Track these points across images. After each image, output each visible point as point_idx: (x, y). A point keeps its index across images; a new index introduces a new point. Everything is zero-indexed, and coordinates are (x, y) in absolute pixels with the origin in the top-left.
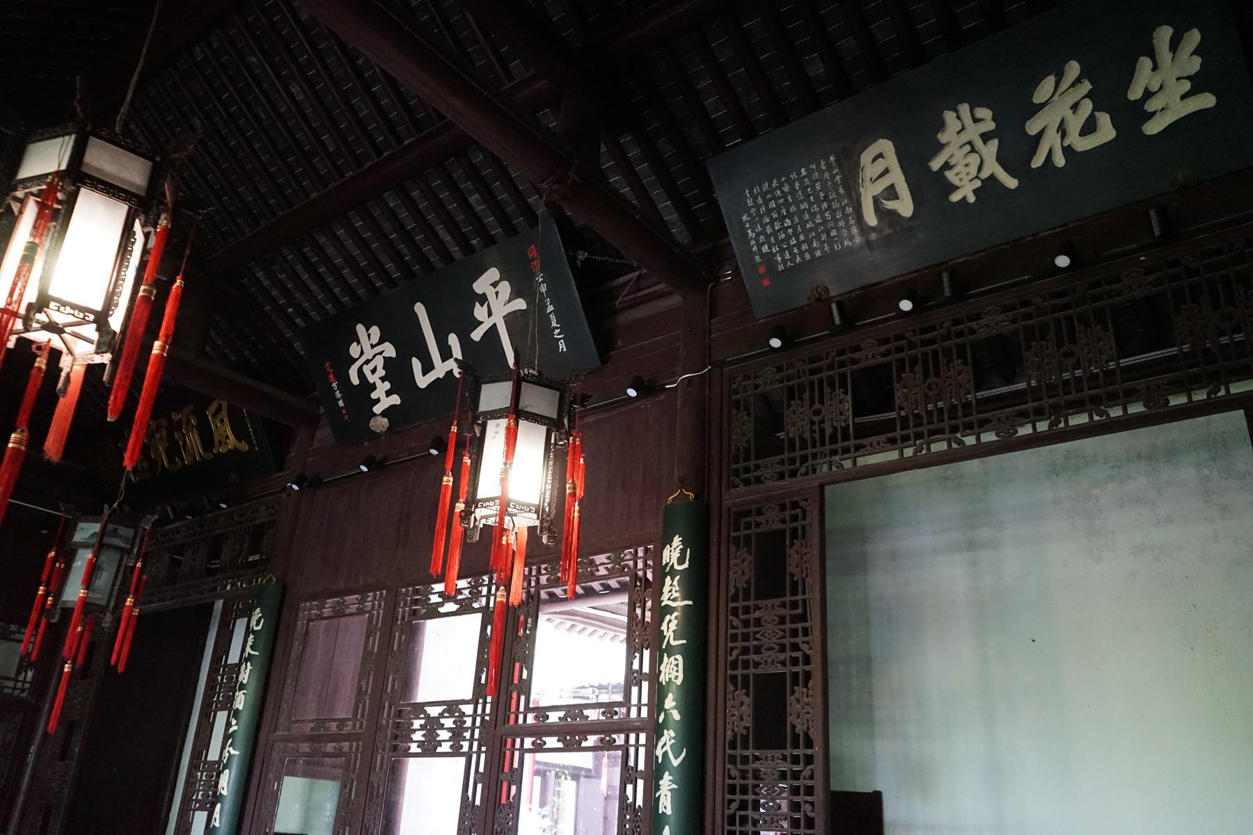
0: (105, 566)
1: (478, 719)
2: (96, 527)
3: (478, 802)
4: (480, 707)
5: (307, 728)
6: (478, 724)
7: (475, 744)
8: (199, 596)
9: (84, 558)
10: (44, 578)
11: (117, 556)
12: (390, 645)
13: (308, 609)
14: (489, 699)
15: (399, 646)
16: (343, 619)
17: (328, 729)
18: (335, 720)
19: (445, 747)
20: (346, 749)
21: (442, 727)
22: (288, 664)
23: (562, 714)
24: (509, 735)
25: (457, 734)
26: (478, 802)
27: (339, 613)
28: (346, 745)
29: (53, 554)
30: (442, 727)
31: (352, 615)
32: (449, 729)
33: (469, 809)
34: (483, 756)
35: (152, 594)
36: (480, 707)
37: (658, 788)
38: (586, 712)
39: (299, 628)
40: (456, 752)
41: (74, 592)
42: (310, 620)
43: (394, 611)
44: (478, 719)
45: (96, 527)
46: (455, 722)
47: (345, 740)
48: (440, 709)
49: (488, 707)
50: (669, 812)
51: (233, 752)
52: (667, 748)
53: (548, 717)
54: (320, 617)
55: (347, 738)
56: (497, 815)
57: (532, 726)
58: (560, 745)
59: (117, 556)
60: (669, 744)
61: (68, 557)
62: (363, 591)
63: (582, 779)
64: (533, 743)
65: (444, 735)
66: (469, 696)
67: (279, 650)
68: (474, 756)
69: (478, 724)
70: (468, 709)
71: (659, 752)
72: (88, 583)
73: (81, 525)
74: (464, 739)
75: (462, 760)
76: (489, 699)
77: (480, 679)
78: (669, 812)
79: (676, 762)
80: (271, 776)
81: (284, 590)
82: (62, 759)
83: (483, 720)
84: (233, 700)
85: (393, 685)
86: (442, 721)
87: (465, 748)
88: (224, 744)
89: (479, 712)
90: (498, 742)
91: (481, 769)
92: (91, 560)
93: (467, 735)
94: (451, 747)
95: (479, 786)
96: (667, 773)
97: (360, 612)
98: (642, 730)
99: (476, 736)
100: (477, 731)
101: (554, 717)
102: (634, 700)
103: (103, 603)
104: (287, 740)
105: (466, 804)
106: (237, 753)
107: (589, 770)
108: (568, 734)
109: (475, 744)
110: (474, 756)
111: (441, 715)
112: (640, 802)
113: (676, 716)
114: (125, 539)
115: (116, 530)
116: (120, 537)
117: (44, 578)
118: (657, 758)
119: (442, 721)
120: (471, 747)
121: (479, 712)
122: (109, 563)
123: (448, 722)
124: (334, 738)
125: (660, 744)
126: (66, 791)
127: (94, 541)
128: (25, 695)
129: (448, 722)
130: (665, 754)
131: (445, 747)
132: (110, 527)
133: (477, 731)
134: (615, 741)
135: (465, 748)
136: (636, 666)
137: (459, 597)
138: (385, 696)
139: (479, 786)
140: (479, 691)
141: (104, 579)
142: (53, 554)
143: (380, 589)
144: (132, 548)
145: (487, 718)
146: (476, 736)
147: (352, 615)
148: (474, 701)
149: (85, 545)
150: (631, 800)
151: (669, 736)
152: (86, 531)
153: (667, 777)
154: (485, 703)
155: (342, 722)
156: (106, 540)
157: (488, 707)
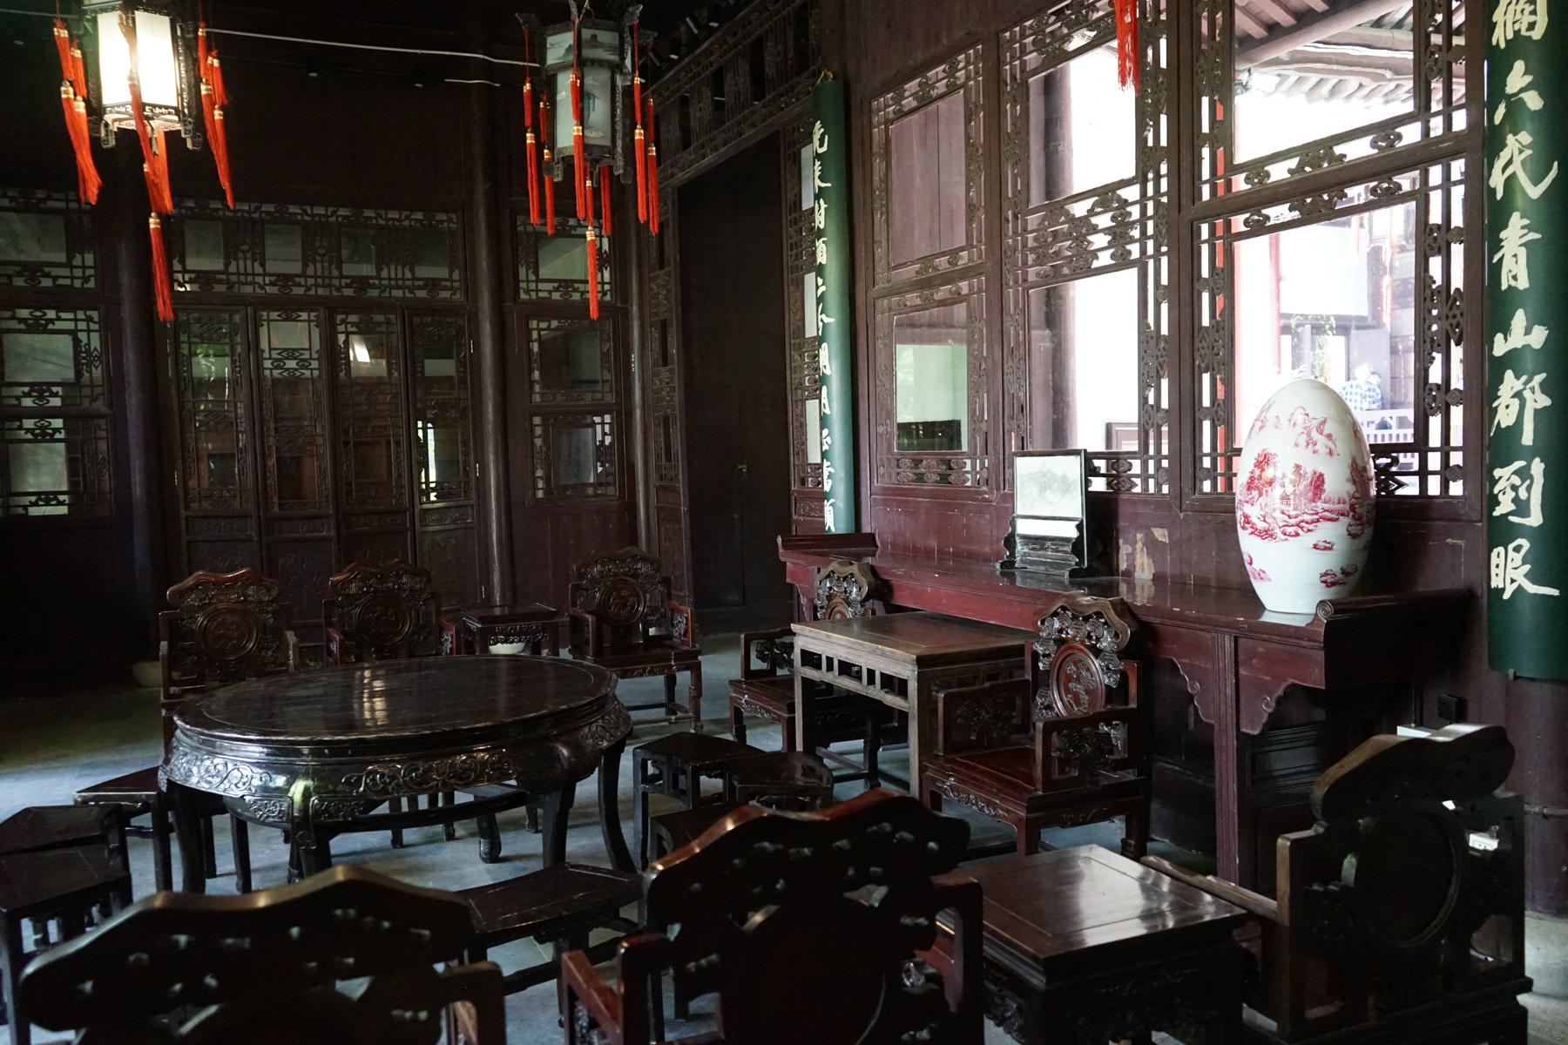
0: (597, 93)
1: (1150, 205)
2: (568, 39)
3: (1164, 331)
4: (1150, 186)
5: (909, 272)
6: (1150, 212)
7: (1150, 244)
8: (752, 131)
9: (566, 81)
10: (528, 121)
11: (605, 75)
12: (1000, 126)
13: (884, 106)
14: (1164, 169)
15: (1014, 125)
16: (932, 107)
17: (935, 269)
18: (943, 254)
19: (1105, 259)
20: (965, 291)
21: (1095, 230)
22: (873, 192)
23: (1293, 163)
24: (1203, 220)
25: (1119, 235)
26: (1164, 331)
27: (925, 101)
28: (964, 286)
29: (527, 87)
30: (1095, 230)
31: (941, 97)
32: (1106, 231)
33: (1152, 343)
34: (1164, 260)
35: (703, 147)
36: (1150, 186)
37: (1497, 245)
38: (1338, 150)
39: (876, 138)
40: (1122, 262)
41: (567, 133)
42: (888, 122)
43: (999, 71)
44: (1150, 205)
45: (568, 39)
46: (1113, 218)
47: (962, 279)
48: (1087, 204)
49: (1164, 183)
50: (1523, 283)
51: (826, 320)
52: (1516, 167)
53: (1268, 175)
54: (901, 114)
55: (966, 273)
56: (1197, 345)
57: (1246, 194)
58: (1296, 214)
59: (605, 75)
60: (1518, 160)
61: (546, 86)
62: (948, 57)
63: (1353, 332)
64: (1246, 223)
65: (1099, 240)
66: (1130, 171)
67: (857, 177)
68: (1151, 263)
69: (1150, 212)
70: (1131, 193)
71: (1497, 181)
72: (581, 118)
73: (550, 40)
74: (1132, 240)
75: (1133, 273)
76: (1164, 169)
77: (1146, 139)
78: (1523, 283)
79: (1535, 192)
80: (880, 344)
81: (847, 88)
82: (665, 364)
83: (1158, 205)
84: (814, 253)
85: (1015, 185)
86: (1094, 220)
87: (1135, 254)
88: (819, 310)
89: (1150, 192)
90: (1185, 232)
91: (1164, 281)
92: (574, 84)
93: (1136, 233)
94: (1113, 256)
95: (1164, 307)
96: (1516, 216)
97: (952, 89)
98: (1455, 155)
99: (1150, 231)
100: (1150, 224)
101: (1279, 172)
102: (1435, 439)
103: (607, 143)
104: (890, 293)
105: (1147, 338)
106: (831, 320)
107: (1363, 319)
108: (1307, 193)
109: (1150, 244)
110: (1151, 263)
111: (1091, 213)
112: (1457, 282)
113: (1534, 101)
114: (611, 49)
115: (594, 36)
116: (602, 46)
117: (528, 121)
118: (1493, 191)
119: (1094, 220)
120: (1143, 251)
121: (1150, 192)
122: (596, 81)
123: (1104, 221)
124: (948, 278)
125: (1499, 164)
126: (676, 399)
127: (571, 58)
128: (608, 298)
129: (1104, 221)
130: (1510, 182)
131: (1105, 259)
132: (587, 34)
133: (1150, 224)
134: (1399, 187)
135: (1135, 254)
136: (1435, 376)
137: (1096, 16)
138: (1005, 204)
139: (1164, 307)
140: (1146, 157)
141: (599, 110)
142: (527, 87)
143: (972, 45)
144: (623, 59)
145: (1164, 200)
146: (1150, 231)
147: (941, 97)
148: (1140, 178)
149: (564, 67)
150: (1439, 282)
151: (1518, 148)
152: (559, 47)
153: (1516, 222)
154: (1158, 177)
155: (954, 254)
156: (588, 53)
157: (1164, 183)
